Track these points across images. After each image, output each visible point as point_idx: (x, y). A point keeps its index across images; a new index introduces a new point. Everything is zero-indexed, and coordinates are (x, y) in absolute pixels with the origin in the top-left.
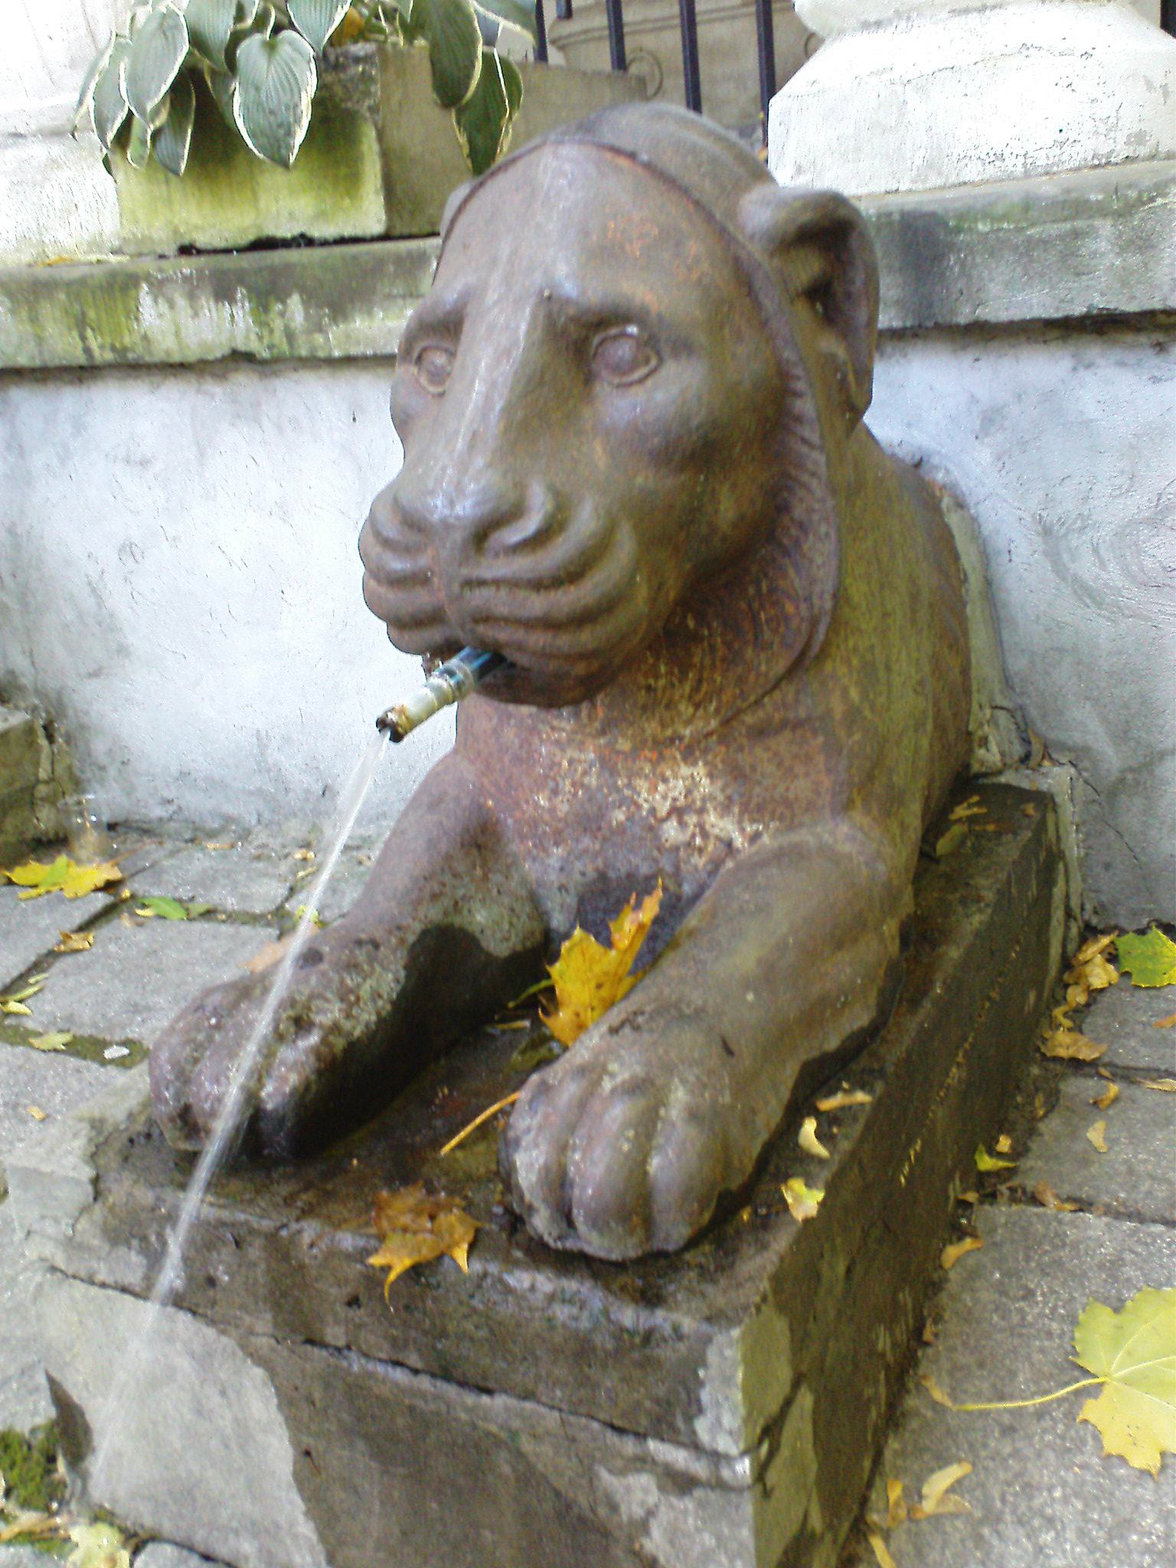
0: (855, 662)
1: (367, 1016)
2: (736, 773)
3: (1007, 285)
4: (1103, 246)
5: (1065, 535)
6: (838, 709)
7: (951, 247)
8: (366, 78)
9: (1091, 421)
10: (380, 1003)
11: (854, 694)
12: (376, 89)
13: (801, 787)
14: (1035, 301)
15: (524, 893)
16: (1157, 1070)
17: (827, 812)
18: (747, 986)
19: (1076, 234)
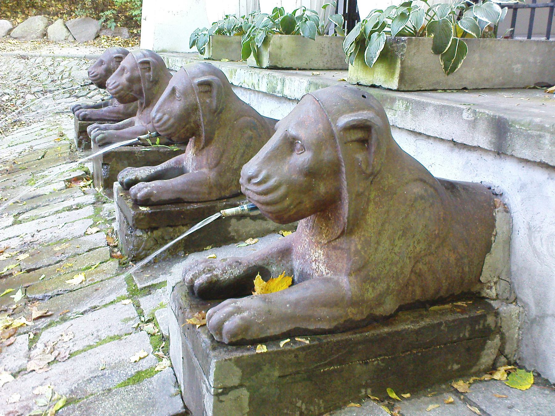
0: (362, 239)
1: (226, 277)
2: (328, 256)
3: (521, 146)
4: (547, 142)
5: (534, 232)
6: (353, 249)
7: (509, 131)
8: (403, 46)
9: (549, 197)
10: (232, 275)
11: (359, 247)
12: (405, 50)
13: (340, 265)
14: (527, 154)
15: (290, 268)
16: (477, 404)
17: (344, 274)
18: (288, 303)
19: (540, 136)
